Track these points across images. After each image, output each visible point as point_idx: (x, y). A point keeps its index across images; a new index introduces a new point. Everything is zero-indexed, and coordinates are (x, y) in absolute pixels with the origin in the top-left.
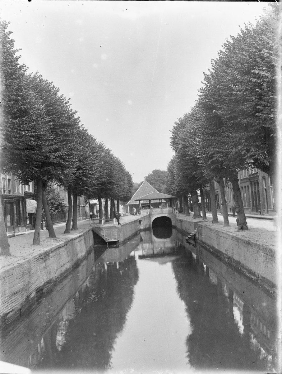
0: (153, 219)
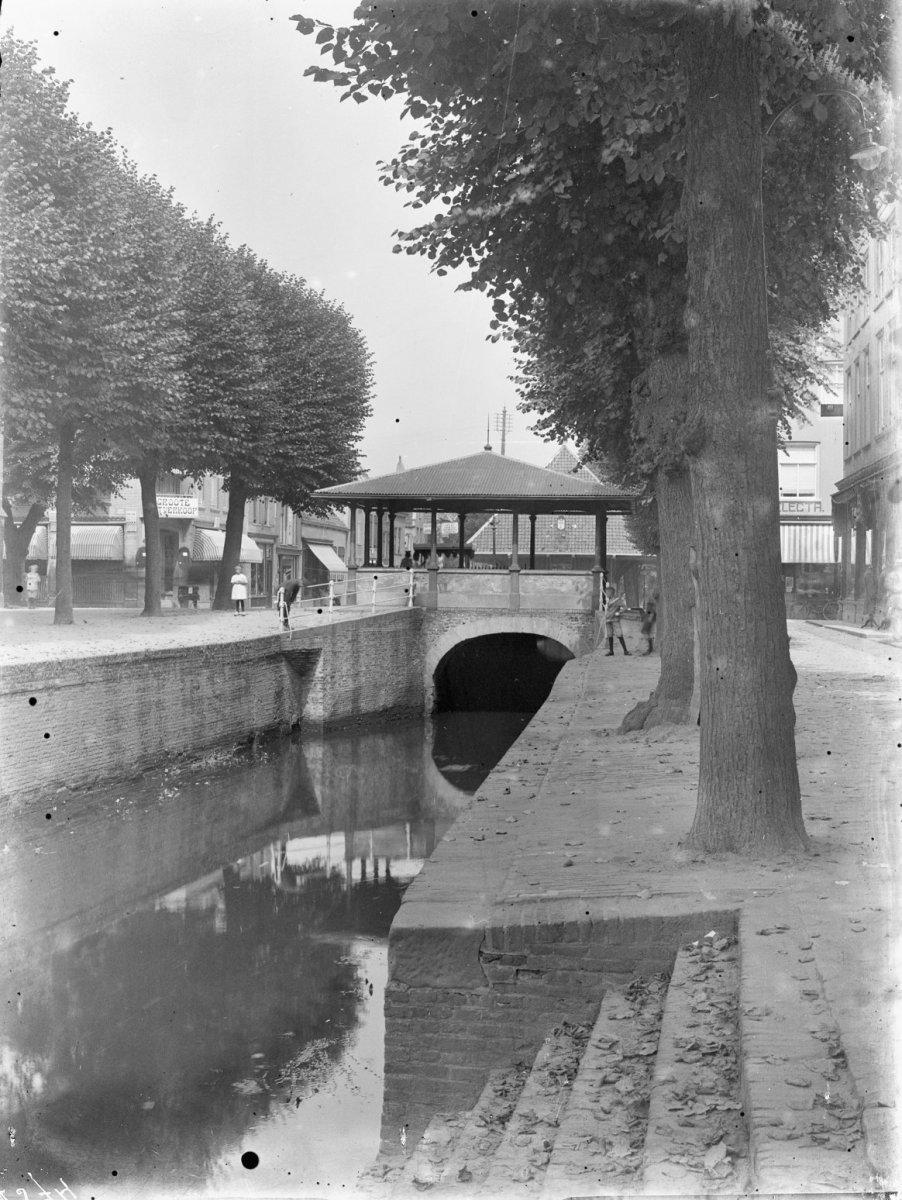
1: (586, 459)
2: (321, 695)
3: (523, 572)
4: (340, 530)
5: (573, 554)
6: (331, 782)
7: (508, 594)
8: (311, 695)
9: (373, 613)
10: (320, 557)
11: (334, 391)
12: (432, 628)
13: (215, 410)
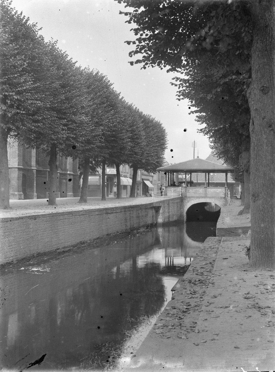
0: (188, 205)
1: (224, 163)
2: (161, 217)
3: (208, 187)
4: (151, 176)
5: (215, 182)
6: (164, 237)
7: (204, 193)
8: (159, 217)
9: (172, 198)
10: (147, 184)
11: (158, 143)
12: (186, 201)
13: (135, 150)
